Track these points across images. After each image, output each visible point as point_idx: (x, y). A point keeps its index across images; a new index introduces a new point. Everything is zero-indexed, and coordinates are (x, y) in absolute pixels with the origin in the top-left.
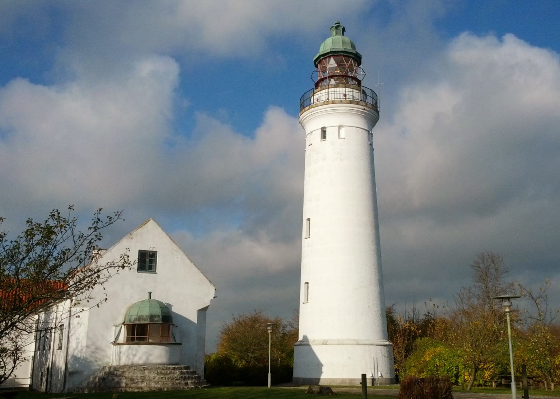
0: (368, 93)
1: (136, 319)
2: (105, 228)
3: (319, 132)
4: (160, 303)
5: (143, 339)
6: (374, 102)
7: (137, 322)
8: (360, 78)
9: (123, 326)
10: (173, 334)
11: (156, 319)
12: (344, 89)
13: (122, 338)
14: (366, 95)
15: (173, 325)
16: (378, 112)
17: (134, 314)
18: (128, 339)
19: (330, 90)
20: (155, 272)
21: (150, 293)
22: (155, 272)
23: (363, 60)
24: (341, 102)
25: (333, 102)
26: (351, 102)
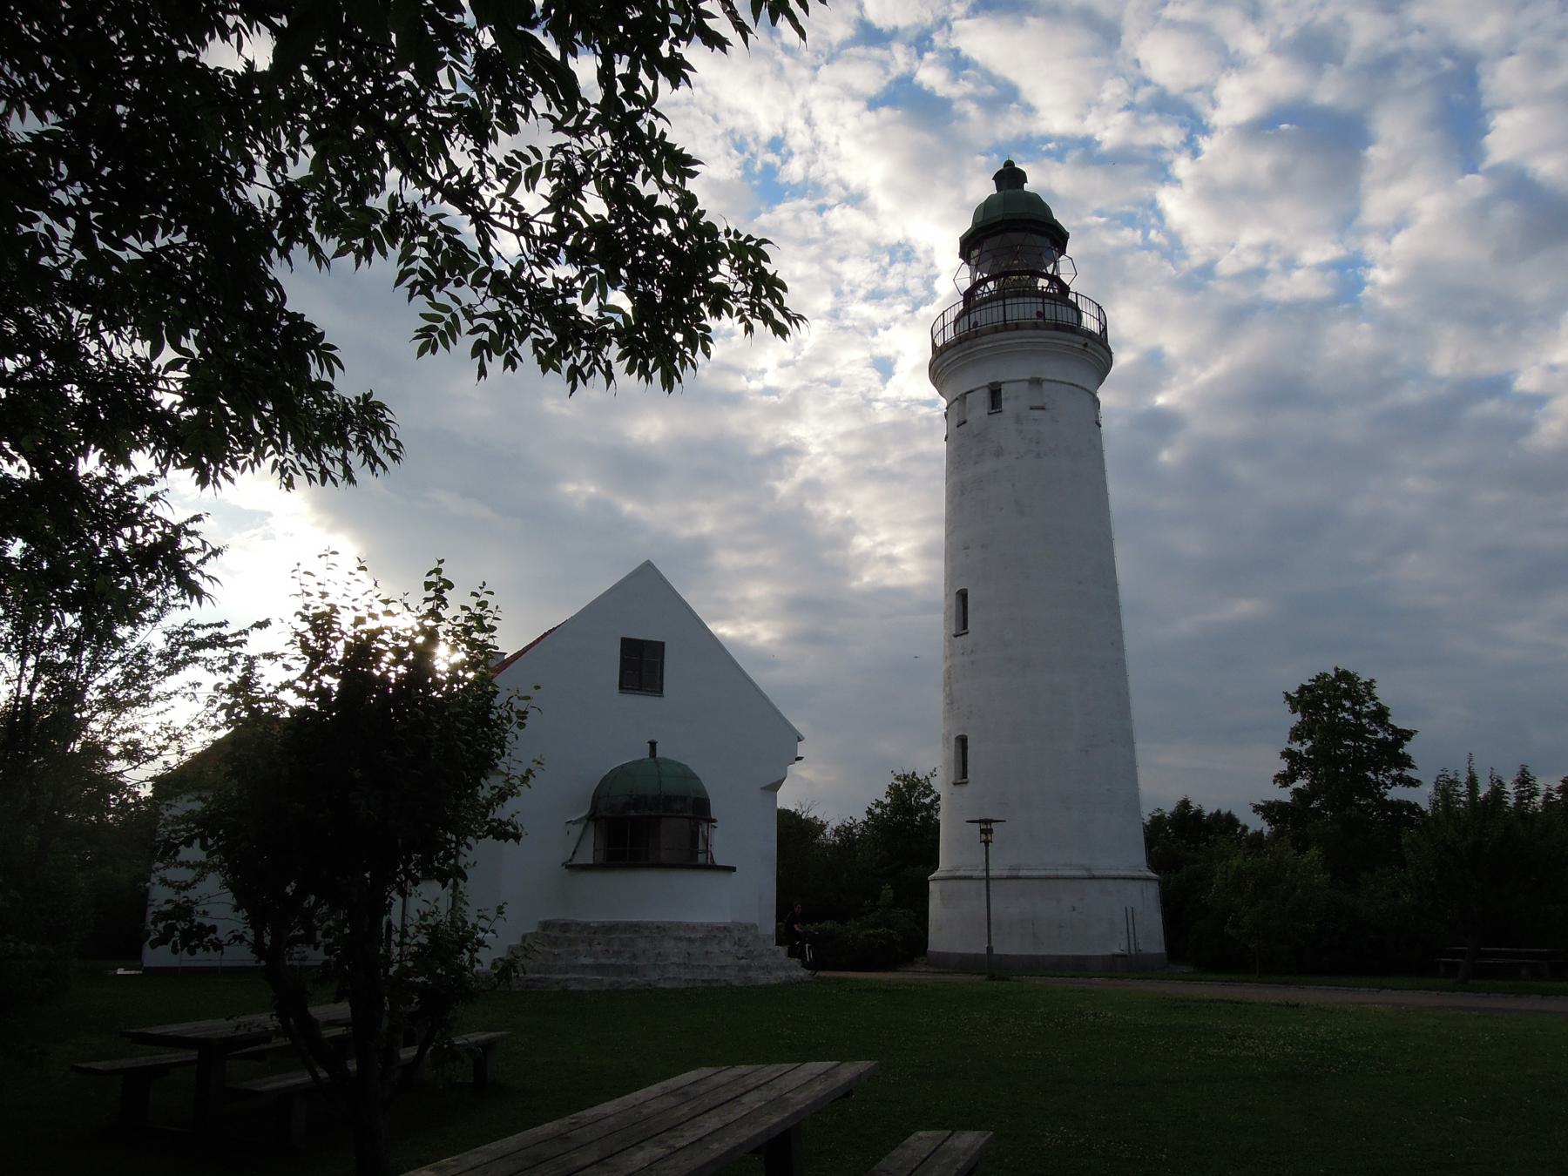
3: (984, 395)
7: (632, 813)
8: (1065, 279)
9: (592, 826)
13: (586, 857)
20: (662, 644)
21: (653, 744)
24: (1036, 326)
25: (1017, 327)
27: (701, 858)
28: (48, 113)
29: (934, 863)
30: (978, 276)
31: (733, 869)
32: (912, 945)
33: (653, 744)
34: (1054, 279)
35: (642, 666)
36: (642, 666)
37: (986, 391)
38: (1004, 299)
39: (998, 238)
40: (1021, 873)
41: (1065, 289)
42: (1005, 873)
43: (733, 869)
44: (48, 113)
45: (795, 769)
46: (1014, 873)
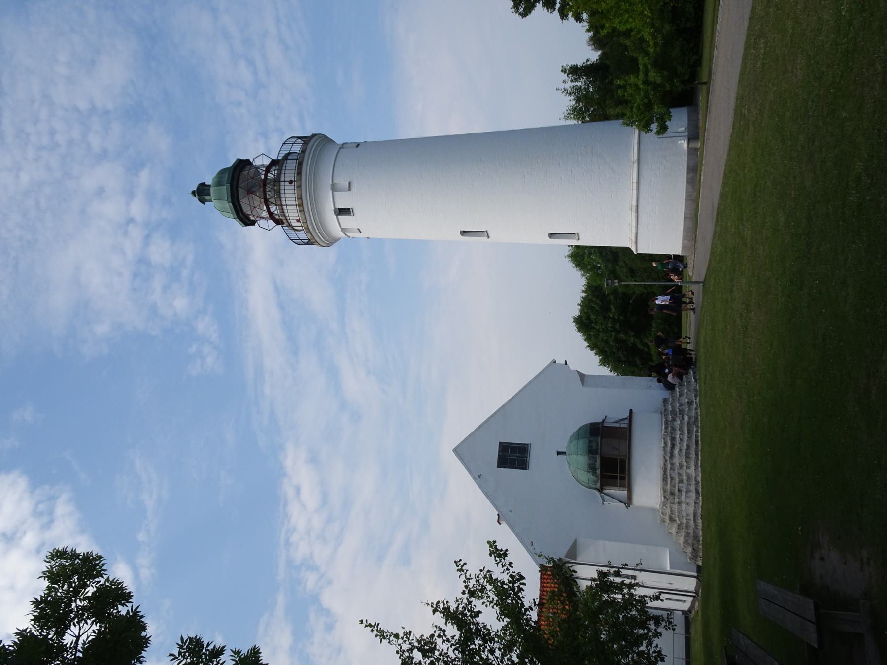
0: (285, 151)
1: (594, 474)
2: (573, 552)
3: (342, 218)
4: (571, 441)
5: (623, 462)
6: (299, 141)
7: (598, 472)
8: (267, 162)
9: (605, 491)
10: (616, 422)
11: (594, 445)
12: (282, 184)
13: (622, 493)
14: (289, 154)
15: (603, 421)
16: (314, 135)
17: (585, 476)
18: (622, 486)
19: (284, 203)
20: (500, 443)
21: (559, 453)
22: (500, 443)
23: (244, 157)
24: (299, 187)
25: (300, 198)
26: (299, 173)
27: (624, 425)
28: (62, 508)
29: (628, 250)
30: (265, 214)
31: (631, 411)
32: (674, 264)
33: (559, 453)
34: (268, 169)
35: (513, 456)
36: (513, 456)
37: (339, 217)
38: (282, 205)
39: (240, 189)
40: (634, 204)
41: (274, 162)
42: (634, 214)
43: (631, 411)
44: (62, 508)
45: (573, 366)
46: (634, 208)
